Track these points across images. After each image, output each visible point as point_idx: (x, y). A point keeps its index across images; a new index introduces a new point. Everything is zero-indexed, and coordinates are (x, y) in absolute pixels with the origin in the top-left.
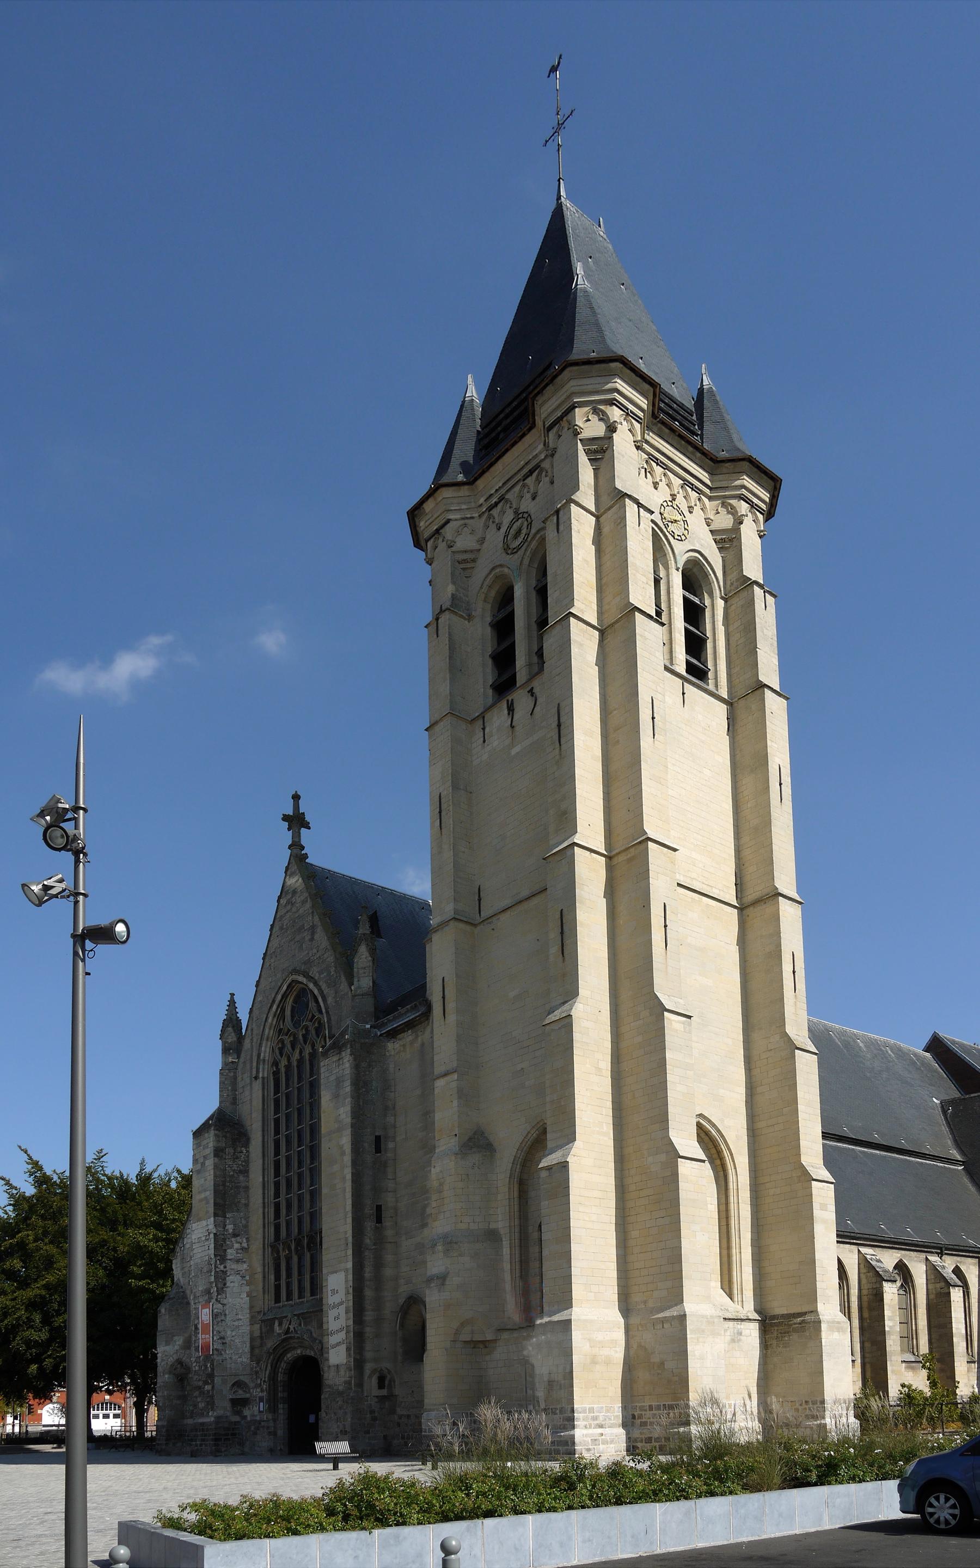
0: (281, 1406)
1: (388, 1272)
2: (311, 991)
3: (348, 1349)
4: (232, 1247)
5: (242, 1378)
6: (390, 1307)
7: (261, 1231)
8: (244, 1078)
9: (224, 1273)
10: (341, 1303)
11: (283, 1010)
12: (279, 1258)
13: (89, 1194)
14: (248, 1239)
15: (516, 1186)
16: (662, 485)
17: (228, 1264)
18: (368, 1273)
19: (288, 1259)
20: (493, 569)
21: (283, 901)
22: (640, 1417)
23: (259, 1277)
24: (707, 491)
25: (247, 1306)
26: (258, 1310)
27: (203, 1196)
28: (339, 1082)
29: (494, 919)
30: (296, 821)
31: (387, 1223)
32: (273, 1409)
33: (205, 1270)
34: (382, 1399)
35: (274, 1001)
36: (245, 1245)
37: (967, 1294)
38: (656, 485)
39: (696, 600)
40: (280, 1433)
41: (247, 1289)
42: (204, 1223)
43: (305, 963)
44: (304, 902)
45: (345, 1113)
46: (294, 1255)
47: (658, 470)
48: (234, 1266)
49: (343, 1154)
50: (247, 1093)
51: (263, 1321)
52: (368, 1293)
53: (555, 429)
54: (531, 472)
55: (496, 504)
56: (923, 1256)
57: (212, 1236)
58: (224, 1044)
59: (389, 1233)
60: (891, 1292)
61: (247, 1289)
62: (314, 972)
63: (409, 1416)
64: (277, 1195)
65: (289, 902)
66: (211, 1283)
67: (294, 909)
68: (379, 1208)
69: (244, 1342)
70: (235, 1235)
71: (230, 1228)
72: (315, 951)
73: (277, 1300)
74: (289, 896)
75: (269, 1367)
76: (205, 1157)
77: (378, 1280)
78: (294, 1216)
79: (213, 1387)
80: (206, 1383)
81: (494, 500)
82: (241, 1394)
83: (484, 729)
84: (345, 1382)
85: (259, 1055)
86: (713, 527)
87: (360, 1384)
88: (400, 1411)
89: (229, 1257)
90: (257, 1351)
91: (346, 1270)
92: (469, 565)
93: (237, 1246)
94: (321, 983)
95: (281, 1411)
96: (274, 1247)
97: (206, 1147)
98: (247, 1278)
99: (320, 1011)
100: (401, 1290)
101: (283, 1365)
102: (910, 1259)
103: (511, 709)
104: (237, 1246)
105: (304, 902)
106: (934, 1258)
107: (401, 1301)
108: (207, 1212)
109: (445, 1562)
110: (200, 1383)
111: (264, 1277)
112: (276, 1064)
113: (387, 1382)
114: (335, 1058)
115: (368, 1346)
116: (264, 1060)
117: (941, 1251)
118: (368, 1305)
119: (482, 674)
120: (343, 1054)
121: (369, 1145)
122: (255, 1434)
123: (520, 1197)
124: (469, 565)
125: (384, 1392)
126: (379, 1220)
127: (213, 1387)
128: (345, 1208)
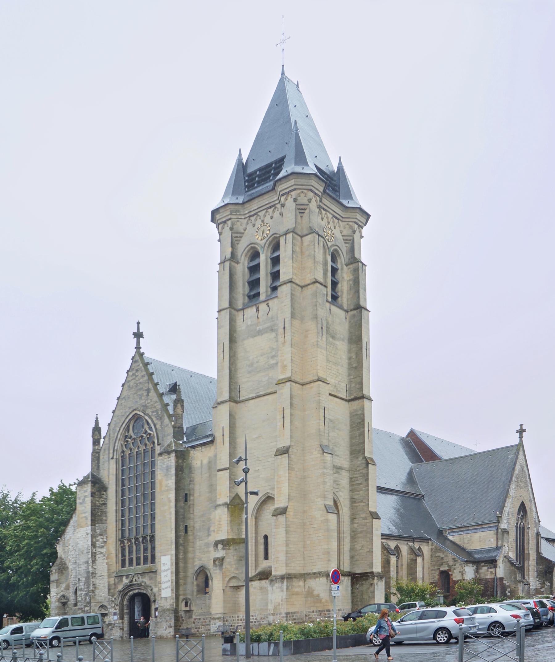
0: (125, 616)
1: (190, 555)
2: (146, 420)
3: (172, 590)
4: (98, 541)
5: (104, 604)
6: (191, 571)
7: (115, 533)
8: (103, 457)
9: (95, 553)
10: (168, 569)
11: (128, 427)
12: (124, 546)
13: (419, 620)
14: (107, 537)
15: (254, 520)
16: (325, 219)
17: (97, 549)
18: (181, 556)
19: (130, 547)
20: (251, 244)
21: (130, 374)
22: (309, 615)
23: (114, 555)
24: (341, 219)
25: (106, 569)
26: (113, 571)
27: (83, 515)
28: (168, 469)
29: (246, 402)
30: (138, 335)
31: (190, 533)
32: (122, 618)
33: (85, 552)
34: (186, 612)
35: (124, 422)
36: (105, 540)
37: (423, 559)
38: (322, 219)
39: (335, 267)
40: (125, 629)
41: (106, 561)
42: (84, 529)
43: (143, 406)
44: (143, 376)
45: (171, 482)
46: (138, 547)
47: (324, 212)
48: (100, 550)
49: (170, 501)
50: (106, 465)
51: (116, 577)
52: (181, 565)
53: (285, 196)
54: (271, 207)
55: (253, 215)
56: (406, 543)
57: (90, 536)
58: (93, 439)
59: (191, 538)
60: (393, 559)
61: (106, 561)
62: (149, 411)
63: (199, 619)
64: (123, 516)
65: (133, 374)
66: (89, 558)
67: (137, 379)
68: (186, 526)
69: (105, 587)
70: (101, 535)
71: (98, 531)
72: (149, 401)
73: (123, 565)
74: (134, 372)
75: (120, 598)
76: (85, 497)
77: (185, 559)
78: (133, 526)
79: (90, 609)
80: (86, 606)
81: (252, 213)
82: (103, 611)
83: (244, 315)
84: (171, 605)
85: (114, 447)
86: (343, 234)
87: (177, 605)
88: (194, 617)
89: (97, 546)
90: (112, 591)
91: (172, 555)
92: (238, 239)
93: (101, 540)
94: (153, 417)
95: (125, 619)
96: (122, 542)
97: (85, 491)
98: (106, 556)
99: (150, 428)
100: (195, 564)
101: (127, 597)
102: (401, 544)
103: (257, 310)
104: (101, 540)
105: (143, 376)
106: (411, 544)
107: (196, 568)
108: (87, 524)
109: (550, 623)
110: (82, 607)
111: (116, 555)
112: (123, 452)
113: (189, 604)
114: (166, 457)
115: (181, 588)
116: (117, 450)
117: (414, 540)
118: (181, 570)
119: (242, 289)
120: (171, 455)
121: (181, 498)
122: (111, 630)
123: (255, 524)
124: (238, 239)
125: (188, 609)
126: (186, 532)
127: (90, 609)
128: (171, 527)
